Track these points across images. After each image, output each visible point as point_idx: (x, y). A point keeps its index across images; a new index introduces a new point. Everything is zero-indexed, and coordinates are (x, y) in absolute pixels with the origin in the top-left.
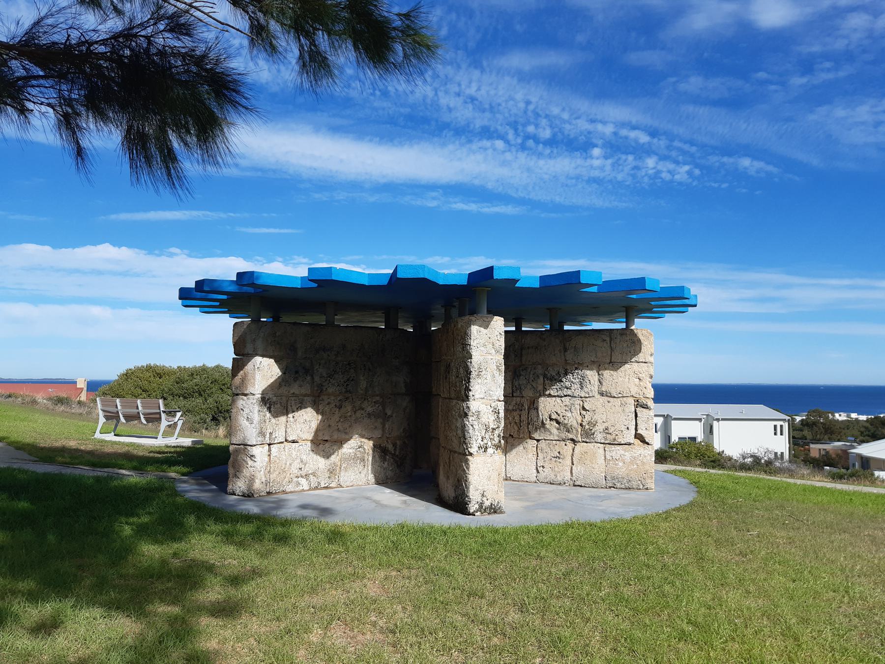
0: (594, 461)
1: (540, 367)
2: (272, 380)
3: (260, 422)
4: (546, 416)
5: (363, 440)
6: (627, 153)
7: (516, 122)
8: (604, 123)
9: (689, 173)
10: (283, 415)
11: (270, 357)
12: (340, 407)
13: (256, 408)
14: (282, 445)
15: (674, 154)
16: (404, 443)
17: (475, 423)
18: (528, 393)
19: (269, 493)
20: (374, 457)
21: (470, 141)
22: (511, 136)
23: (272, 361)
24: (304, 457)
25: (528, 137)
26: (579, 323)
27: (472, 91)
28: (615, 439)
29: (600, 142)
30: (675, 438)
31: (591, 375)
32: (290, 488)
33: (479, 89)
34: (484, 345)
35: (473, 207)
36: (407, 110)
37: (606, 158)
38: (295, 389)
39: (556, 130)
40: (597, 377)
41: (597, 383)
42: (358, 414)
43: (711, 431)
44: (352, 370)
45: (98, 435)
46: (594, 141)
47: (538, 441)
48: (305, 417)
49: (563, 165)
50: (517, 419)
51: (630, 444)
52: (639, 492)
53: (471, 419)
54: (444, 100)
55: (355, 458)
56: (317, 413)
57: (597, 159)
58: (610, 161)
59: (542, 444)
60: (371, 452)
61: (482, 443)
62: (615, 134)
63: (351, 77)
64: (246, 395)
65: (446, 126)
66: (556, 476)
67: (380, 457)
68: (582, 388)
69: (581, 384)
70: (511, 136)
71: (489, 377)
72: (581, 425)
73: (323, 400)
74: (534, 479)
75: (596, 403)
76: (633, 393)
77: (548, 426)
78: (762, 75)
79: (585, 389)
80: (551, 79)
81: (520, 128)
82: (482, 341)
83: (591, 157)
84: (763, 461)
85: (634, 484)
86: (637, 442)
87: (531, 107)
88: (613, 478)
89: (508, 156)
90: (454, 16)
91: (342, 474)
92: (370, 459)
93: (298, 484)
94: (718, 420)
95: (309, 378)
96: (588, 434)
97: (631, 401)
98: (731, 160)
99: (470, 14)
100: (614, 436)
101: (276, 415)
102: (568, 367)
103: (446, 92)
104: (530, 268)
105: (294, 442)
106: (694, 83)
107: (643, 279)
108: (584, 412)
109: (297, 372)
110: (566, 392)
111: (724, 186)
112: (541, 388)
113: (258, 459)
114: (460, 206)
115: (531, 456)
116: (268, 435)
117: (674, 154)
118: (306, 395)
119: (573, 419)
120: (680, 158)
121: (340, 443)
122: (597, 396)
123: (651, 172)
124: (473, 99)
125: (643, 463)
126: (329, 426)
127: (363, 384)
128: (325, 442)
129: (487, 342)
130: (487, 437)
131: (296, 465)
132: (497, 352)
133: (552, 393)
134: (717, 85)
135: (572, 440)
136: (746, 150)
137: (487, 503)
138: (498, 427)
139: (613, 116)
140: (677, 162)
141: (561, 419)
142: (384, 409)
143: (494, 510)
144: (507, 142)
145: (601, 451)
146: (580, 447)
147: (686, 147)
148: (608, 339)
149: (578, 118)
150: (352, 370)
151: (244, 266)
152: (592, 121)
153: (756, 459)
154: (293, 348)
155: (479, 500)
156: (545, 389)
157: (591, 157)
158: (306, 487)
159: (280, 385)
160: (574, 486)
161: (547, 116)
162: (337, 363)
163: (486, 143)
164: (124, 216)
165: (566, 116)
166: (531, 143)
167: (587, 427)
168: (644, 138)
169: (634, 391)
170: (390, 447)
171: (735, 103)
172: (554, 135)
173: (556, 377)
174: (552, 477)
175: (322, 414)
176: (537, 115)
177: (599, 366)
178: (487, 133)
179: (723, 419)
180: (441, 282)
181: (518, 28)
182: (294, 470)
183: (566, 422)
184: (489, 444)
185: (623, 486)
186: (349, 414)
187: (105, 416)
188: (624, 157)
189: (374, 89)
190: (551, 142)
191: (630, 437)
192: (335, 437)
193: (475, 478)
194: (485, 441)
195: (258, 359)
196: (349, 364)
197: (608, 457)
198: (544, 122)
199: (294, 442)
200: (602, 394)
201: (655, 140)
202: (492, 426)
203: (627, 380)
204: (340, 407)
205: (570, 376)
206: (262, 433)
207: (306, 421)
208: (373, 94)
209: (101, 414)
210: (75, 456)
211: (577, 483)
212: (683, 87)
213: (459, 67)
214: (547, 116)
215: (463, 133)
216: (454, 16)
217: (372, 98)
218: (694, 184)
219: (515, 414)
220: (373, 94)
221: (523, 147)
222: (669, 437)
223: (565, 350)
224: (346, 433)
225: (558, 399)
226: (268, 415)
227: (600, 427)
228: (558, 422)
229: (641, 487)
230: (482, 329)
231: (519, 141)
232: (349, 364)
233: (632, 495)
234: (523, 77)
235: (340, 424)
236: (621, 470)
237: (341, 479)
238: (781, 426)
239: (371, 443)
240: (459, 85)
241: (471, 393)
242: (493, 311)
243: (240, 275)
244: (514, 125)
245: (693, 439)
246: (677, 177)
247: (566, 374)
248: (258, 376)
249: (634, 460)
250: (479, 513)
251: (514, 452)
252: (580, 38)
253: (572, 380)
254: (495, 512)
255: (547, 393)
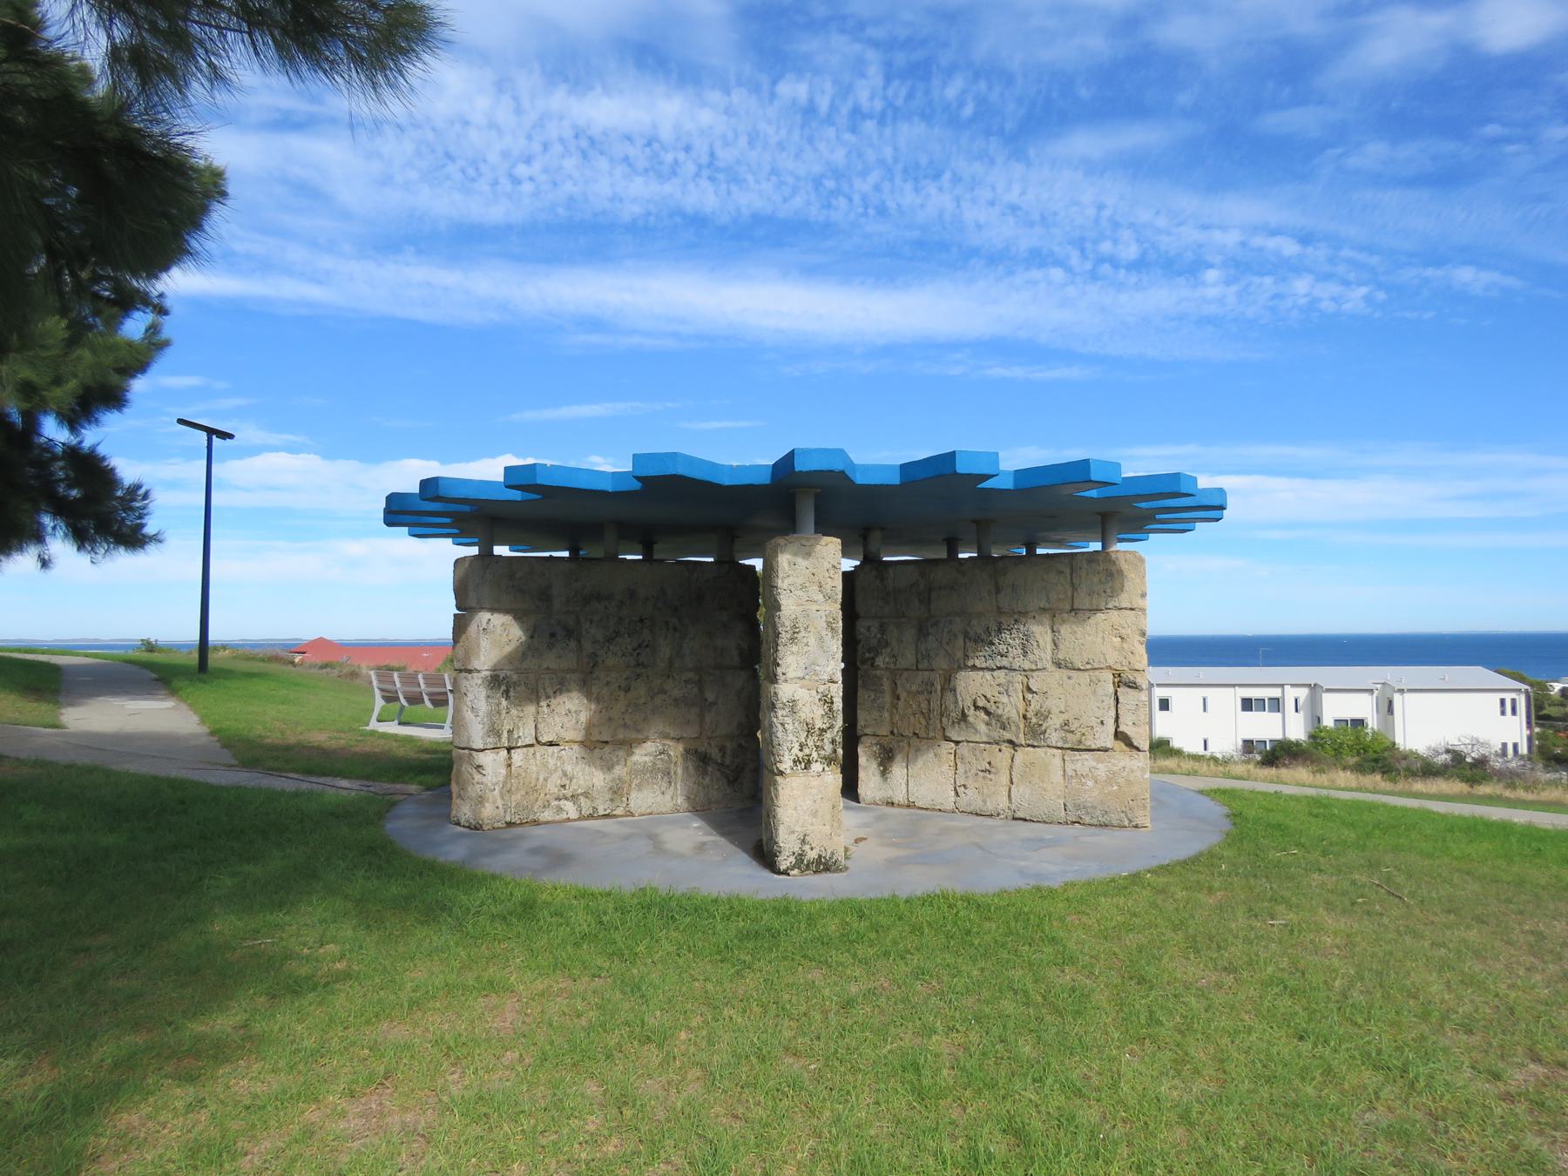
0: (1045, 779)
1: (958, 620)
2: (508, 649)
3: (490, 714)
4: (969, 703)
5: (668, 742)
6: (1261, 274)
7: (1082, 239)
8: (1224, 228)
9: (1368, 299)
10: (531, 701)
11: (507, 612)
12: (627, 690)
13: (483, 693)
14: (531, 750)
15: (1341, 269)
16: (740, 746)
17: (788, 720)
18: (941, 663)
19: (510, 824)
20: (686, 769)
21: (1011, 273)
22: (1075, 260)
23: (507, 619)
24: (569, 769)
25: (1101, 260)
26: (1060, 543)
27: (1014, 196)
28: (1080, 742)
29: (1218, 259)
30: (1328, 722)
31: (1040, 632)
32: (547, 815)
33: (1023, 193)
34: (803, 587)
35: (1017, 372)
36: (916, 234)
37: (1227, 283)
38: (550, 660)
39: (1146, 245)
40: (1049, 637)
41: (1049, 646)
42: (658, 700)
43: (1390, 710)
44: (646, 631)
45: (374, 725)
46: (1209, 258)
47: (957, 743)
48: (569, 705)
49: (1162, 296)
50: (924, 706)
51: (1106, 750)
52: (1118, 833)
53: (780, 713)
54: (971, 214)
55: (654, 770)
56: (589, 700)
57: (1214, 285)
58: (1234, 288)
59: (964, 749)
60: (680, 760)
61: (800, 754)
62: (1243, 244)
63: (832, 192)
64: (470, 671)
65: (974, 252)
66: (985, 802)
67: (697, 768)
68: (1025, 653)
69: (1024, 647)
70: (1075, 260)
71: (812, 641)
72: (1025, 717)
73: (598, 678)
74: (950, 806)
75: (1049, 681)
76: (1111, 662)
77: (971, 719)
78: (1491, 130)
79: (1030, 656)
80: (1137, 166)
81: (1089, 246)
82: (799, 581)
83: (1204, 284)
84: (1469, 760)
85: (1114, 818)
86: (1120, 745)
87: (1106, 213)
88: (1078, 807)
89: (1071, 291)
90: (983, 85)
91: (633, 795)
92: (680, 771)
93: (560, 809)
94: (1401, 691)
95: (573, 644)
96: (1036, 733)
97: (1108, 676)
98: (1440, 273)
99: (1009, 79)
100: (1078, 735)
101: (521, 701)
102: (1003, 620)
103: (974, 201)
104: (878, 451)
105: (551, 744)
106: (1374, 153)
107: (952, 455)
108: (1029, 696)
109: (552, 635)
110: (999, 661)
111: (1428, 315)
112: (960, 655)
113: (488, 770)
114: (998, 372)
115: (947, 769)
116: (505, 734)
117: (1341, 269)
118: (570, 671)
119: (1011, 706)
120: (1352, 276)
121: (628, 745)
122: (1050, 666)
123: (1302, 301)
124: (1014, 208)
125: (1129, 782)
126: (610, 719)
127: (665, 650)
128: (600, 744)
129: (808, 582)
130: (810, 743)
131: (556, 780)
132: (828, 597)
133: (978, 663)
134: (1415, 153)
135: (1011, 742)
136: (1470, 255)
137: (812, 855)
138: (831, 727)
139: (1239, 216)
140: (1346, 283)
141: (992, 708)
142: (701, 691)
143: (824, 865)
144: (1069, 269)
145: (1058, 762)
146: (1020, 755)
147: (1362, 257)
148: (1068, 571)
149: (1181, 224)
150: (646, 631)
151: (432, 469)
152: (1206, 227)
153: (1457, 757)
154: (545, 596)
155: (796, 849)
156: (966, 657)
157: (1204, 284)
158: (573, 815)
159: (524, 656)
160: (1014, 819)
161: (1131, 225)
162: (621, 619)
163: (1036, 274)
164: (530, 415)
165: (1162, 222)
166: (1106, 268)
167: (1034, 720)
168: (1290, 248)
169: (1113, 658)
170: (714, 753)
171: (1445, 179)
172: (1144, 254)
173: (984, 636)
174: (977, 805)
175: (598, 700)
176: (1116, 225)
177: (1053, 614)
178: (1038, 258)
179: (1410, 691)
180: (727, 482)
181: (1084, 93)
182: (552, 787)
183: (1000, 712)
184: (815, 755)
185: (1095, 821)
186: (642, 700)
187: (384, 697)
188: (1257, 280)
189: (866, 207)
190: (1139, 265)
191: (1106, 737)
192: (621, 736)
193: (790, 811)
194: (807, 751)
195: (484, 616)
196: (641, 621)
197: (1069, 772)
198: (1126, 234)
199: (551, 744)
200: (1058, 665)
201: (1310, 250)
202: (819, 724)
203: (1099, 640)
204: (627, 690)
205: (1006, 635)
206: (494, 731)
207: (569, 713)
208: (865, 214)
209: (378, 694)
210: (321, 762)
211: (1019, 814)
212: (1353, 162)
213: (992, 162)
214: (1131, 225)
215: (1000, 260)
216: (983, 85)
217: (863, 220)
218: (1377, 315)
219: (921, 698)
220: (865, 214)
221: (1094, 276)
222: (1319, 720)
223: (998, 590)
224: (638, 731)
225: (988, 675)
226: (504, 703)
227: (1055, 721)
228: (988, 713)
229: (1126, 823)
230: (799, 560)
231: (1088, 266)
232: (641, 621)
233: (1105, 838)
234: (1092, 168)
235: (627, 717)
236: (1091, 793)
237: (632, 804)
238: (1514, 701)
239: (681, 748)
240: (993, 188)
241: (779, 670)
242: (824, 527)
243: (424, 484)
244: (1080, 244)
245: (1359, 723)
246: (1345, 306)
247: (1000, 631)
248: (485, 643)
249: (1112, 778)
250: (796, 871)
251: (920, 763)
252: (1184, 99)
253: (1010, 641)
254: (827, 869)
255: (970, 663)
